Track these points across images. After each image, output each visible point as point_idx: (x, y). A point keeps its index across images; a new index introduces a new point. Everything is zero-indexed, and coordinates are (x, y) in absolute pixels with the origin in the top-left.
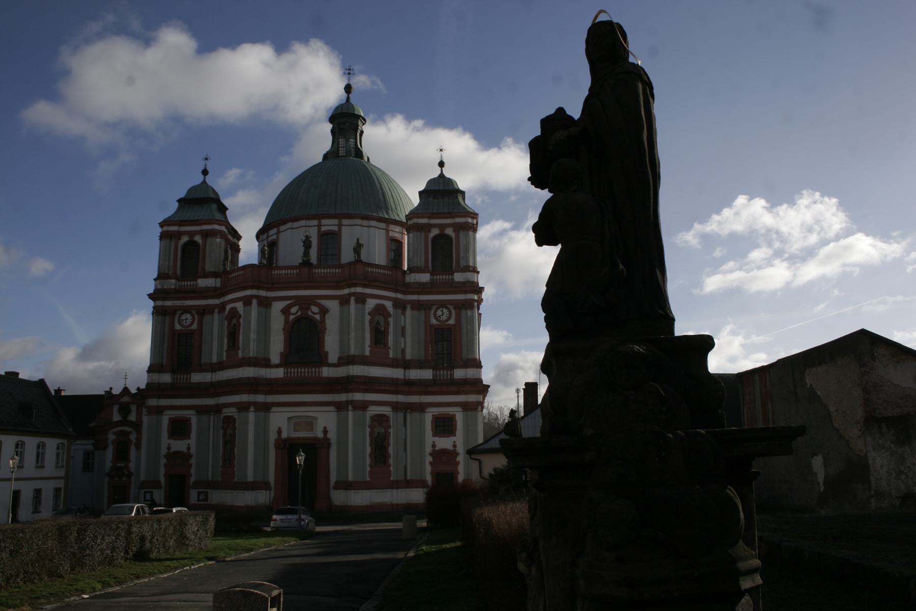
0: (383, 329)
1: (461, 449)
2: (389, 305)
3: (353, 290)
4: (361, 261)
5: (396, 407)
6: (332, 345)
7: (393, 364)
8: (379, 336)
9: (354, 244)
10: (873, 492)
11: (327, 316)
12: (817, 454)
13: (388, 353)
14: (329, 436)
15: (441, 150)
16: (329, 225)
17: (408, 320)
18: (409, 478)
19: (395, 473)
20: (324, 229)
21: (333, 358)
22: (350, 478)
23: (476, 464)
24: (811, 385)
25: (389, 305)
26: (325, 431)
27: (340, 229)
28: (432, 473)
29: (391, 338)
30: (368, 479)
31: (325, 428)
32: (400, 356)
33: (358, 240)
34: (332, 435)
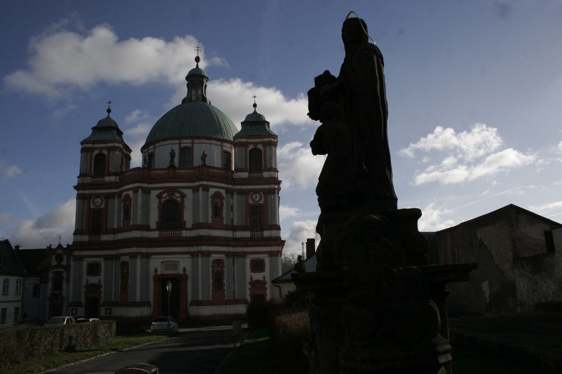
0: (219, 207)
1: (268, 280)
2: (223, 192)
3: (201, 183)
4: (206, 165)
5: (228, 254)
6: (188, 217)
7: (227, 228)
8: (217, 211)
9: (201, 155)
10: (518, 303)
11: (185, 199)
12: (485, 280)
13: (223, 222)
14: (187, 273)
15: (255, 97)
16: (186, 143)
17: (235, 201)
18: (236, 298)
19: (228, 295)
20: (182, 145)
21: (189, 225)
22: (200, 299)
23: (278, 288)
24: (481, 238)
25: (223, 192)
26: (184, 270)
27: (193, 146)
28: (250, 295)
29: (224, 212)
30: (211, 299)
31: (184, 268)
32: (230, 223)
33: (204, 152)
34: (189, 273)
